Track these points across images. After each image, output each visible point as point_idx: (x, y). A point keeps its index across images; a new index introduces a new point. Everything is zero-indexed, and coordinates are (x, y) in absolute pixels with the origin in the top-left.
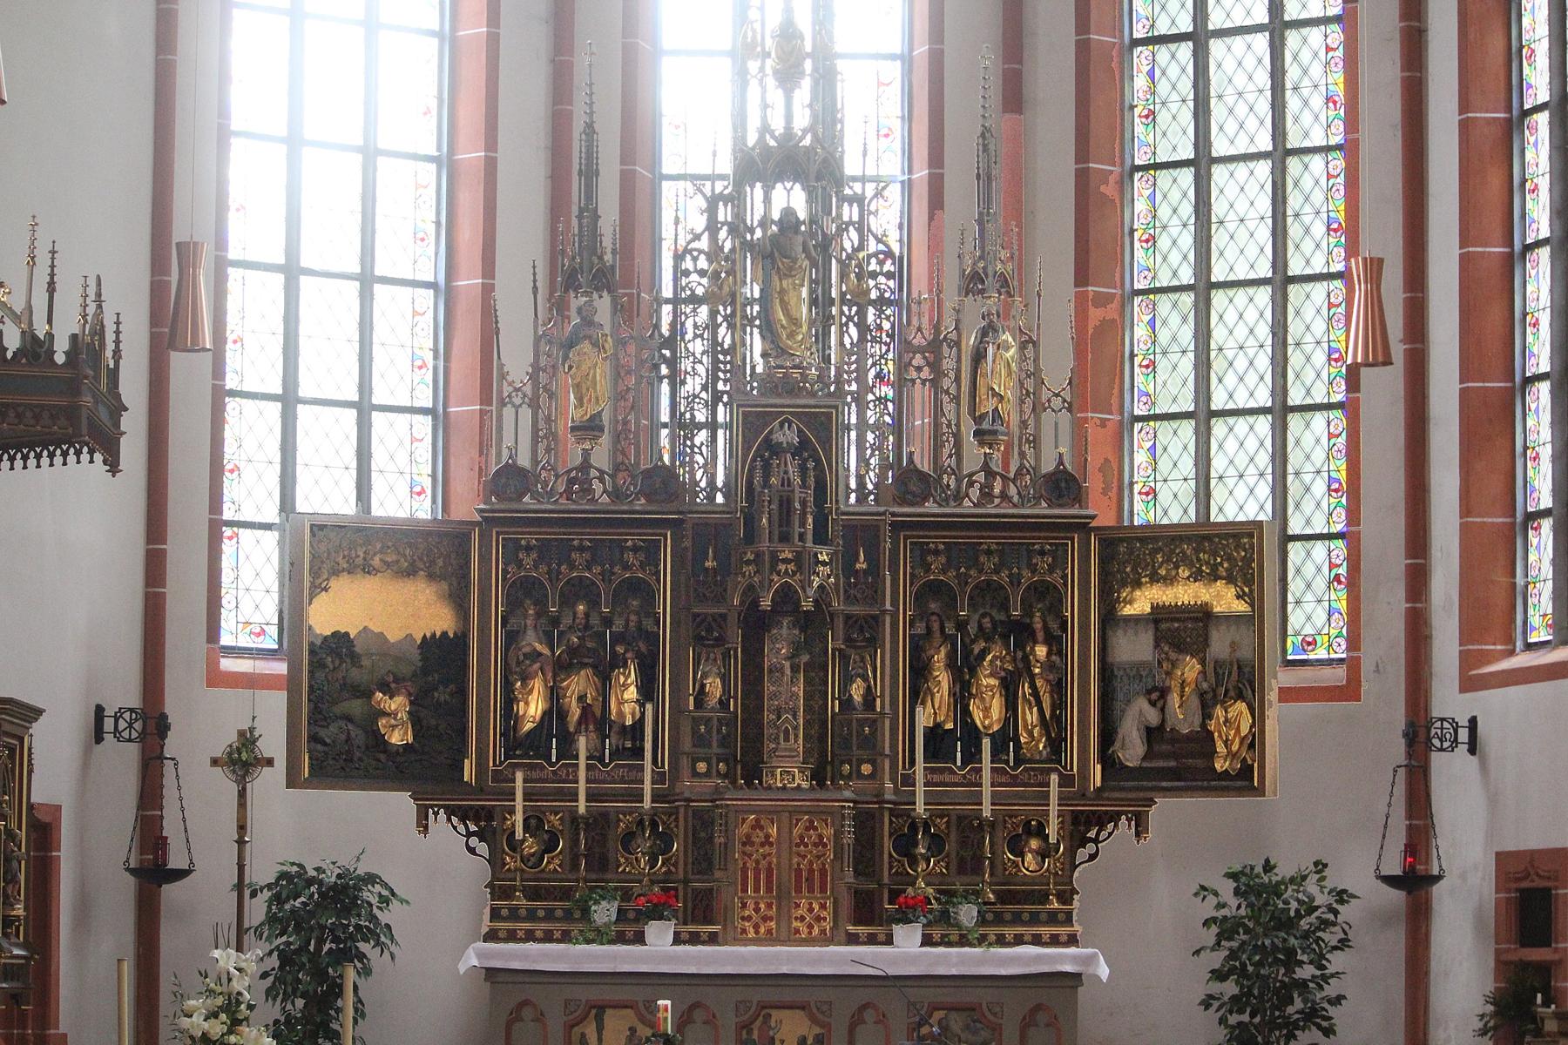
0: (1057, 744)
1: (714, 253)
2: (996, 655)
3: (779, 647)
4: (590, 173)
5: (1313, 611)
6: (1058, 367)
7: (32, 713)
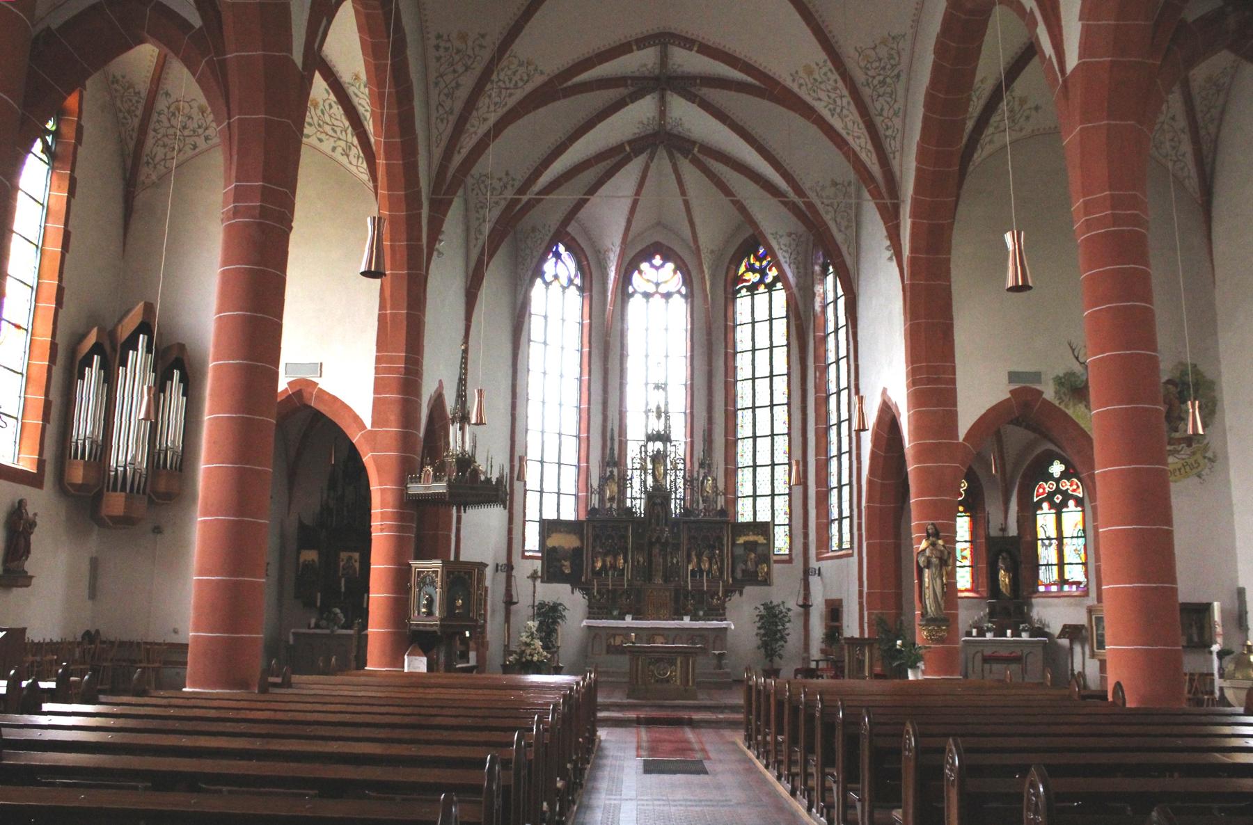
0: (721, 573)
3: (656, 550)
4: (612, 439)
5: (781, 542)
6: (721, 486)
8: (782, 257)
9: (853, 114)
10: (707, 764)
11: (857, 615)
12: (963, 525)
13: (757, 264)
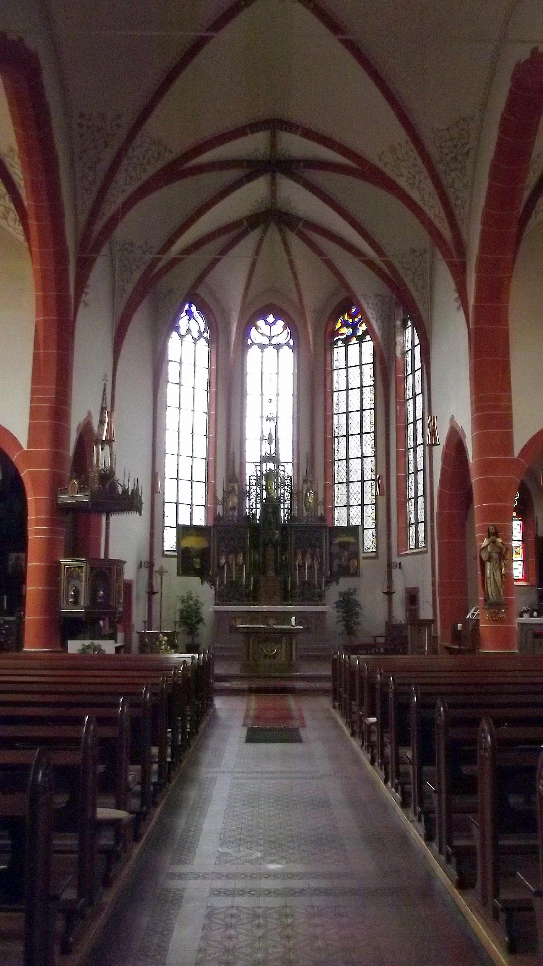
1: (257, 476)
2: (309, 551)
4: (234, 461)
5: (369, 541)
6: (321, 497)
7: (124, 562)
8: (370, 313)
9: (428, 186)
10: (303, 733)
11: (430, 600)
12: (517, 526)
13: (351, 321)
